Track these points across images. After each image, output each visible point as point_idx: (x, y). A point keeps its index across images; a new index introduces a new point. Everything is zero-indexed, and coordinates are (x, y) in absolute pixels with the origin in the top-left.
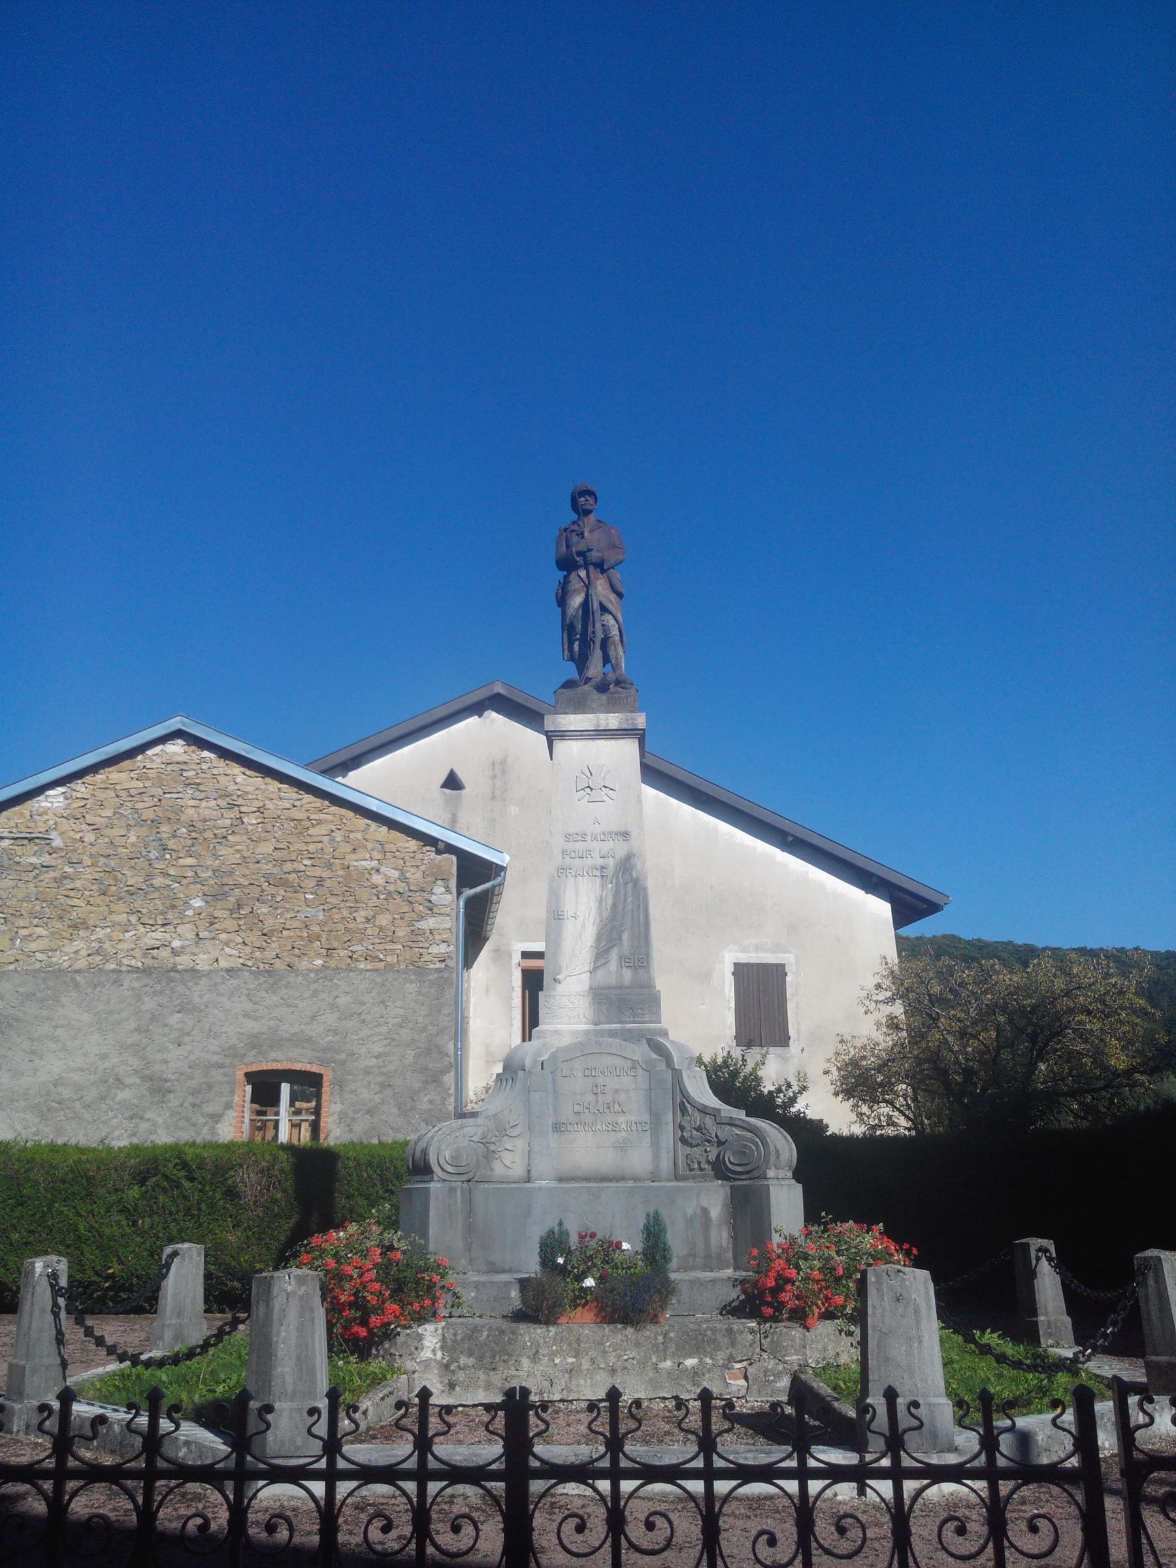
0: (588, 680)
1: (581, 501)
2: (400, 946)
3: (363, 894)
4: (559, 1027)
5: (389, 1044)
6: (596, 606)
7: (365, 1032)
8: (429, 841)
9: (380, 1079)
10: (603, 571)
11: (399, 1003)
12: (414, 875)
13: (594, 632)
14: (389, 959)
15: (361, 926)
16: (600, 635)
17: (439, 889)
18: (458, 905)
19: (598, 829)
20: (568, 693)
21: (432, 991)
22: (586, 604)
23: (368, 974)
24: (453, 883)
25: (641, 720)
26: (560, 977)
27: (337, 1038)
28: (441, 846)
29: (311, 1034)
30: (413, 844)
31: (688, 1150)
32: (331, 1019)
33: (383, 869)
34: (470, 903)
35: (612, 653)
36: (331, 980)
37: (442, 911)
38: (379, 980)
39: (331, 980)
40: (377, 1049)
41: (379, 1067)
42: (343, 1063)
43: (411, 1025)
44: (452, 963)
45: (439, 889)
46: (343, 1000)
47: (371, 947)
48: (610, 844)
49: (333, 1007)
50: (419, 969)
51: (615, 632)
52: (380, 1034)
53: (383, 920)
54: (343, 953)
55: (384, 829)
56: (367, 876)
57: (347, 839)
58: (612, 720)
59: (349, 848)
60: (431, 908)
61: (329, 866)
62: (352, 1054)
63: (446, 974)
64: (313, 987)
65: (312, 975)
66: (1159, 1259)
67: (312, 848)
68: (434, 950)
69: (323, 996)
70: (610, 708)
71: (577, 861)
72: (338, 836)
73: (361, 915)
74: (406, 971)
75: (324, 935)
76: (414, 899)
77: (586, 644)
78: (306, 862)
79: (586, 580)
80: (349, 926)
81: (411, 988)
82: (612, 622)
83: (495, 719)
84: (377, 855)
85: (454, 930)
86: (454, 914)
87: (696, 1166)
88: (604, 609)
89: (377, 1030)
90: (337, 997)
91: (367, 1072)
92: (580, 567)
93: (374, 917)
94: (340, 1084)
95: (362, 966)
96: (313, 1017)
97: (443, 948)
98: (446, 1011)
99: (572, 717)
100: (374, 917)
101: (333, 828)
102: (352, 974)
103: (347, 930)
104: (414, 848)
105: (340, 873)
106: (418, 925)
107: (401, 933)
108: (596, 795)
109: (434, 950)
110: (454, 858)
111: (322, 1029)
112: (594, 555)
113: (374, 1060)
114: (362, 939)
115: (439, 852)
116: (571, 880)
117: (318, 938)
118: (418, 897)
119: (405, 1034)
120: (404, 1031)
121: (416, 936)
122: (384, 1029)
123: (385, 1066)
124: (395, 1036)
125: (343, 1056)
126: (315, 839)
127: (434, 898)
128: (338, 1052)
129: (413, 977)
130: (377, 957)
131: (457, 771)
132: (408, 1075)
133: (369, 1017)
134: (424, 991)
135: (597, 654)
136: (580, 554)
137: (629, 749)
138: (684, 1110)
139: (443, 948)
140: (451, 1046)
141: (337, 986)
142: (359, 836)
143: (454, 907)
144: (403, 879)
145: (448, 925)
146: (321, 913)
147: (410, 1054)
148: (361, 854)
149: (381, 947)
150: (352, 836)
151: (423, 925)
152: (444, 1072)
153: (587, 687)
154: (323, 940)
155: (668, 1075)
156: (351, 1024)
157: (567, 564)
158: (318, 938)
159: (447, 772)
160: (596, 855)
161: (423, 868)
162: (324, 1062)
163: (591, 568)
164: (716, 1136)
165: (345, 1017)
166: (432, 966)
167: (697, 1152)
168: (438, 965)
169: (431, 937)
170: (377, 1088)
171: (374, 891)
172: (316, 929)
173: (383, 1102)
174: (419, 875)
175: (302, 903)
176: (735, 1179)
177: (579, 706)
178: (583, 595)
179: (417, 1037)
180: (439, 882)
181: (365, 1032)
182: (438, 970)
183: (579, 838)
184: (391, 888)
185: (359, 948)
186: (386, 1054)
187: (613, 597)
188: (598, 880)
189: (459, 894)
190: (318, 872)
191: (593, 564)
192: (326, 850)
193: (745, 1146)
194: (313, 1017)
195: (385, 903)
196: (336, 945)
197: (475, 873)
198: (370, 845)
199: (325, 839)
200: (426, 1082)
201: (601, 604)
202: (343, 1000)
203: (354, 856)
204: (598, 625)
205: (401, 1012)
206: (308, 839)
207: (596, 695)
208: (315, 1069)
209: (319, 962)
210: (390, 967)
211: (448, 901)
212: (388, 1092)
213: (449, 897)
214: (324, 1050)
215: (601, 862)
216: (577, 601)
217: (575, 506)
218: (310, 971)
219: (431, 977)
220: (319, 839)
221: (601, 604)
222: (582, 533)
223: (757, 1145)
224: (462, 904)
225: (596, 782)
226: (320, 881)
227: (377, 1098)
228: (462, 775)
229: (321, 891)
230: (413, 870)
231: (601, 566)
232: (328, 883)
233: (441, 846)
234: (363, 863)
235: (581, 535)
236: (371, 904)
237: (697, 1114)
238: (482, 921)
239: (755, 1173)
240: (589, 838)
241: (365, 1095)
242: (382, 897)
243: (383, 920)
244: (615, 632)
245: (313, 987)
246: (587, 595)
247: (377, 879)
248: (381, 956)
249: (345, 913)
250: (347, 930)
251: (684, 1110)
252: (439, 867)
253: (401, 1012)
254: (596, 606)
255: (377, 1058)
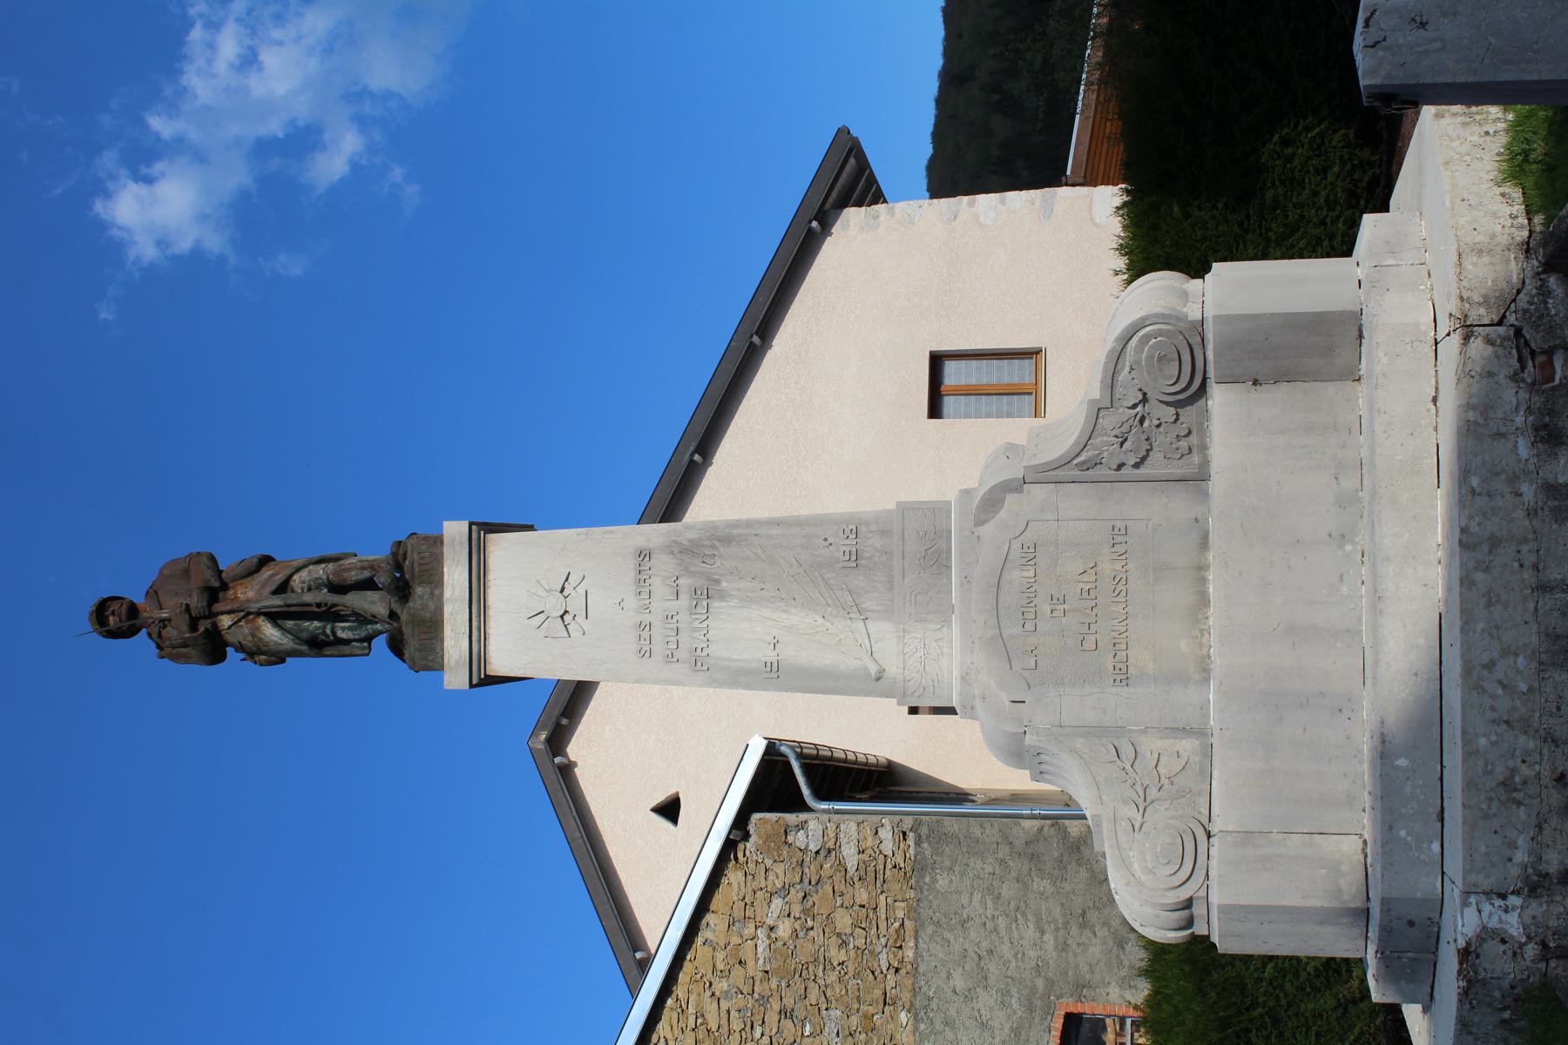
0: (393, 615)
1: (117, 619)
2: (882, 898)
3: (805, 951)
4: (955, 673)
5: (1024, 915)
6: (277, 601)
7: (1006, 950)
8: (729, 847)
9: (1074, 929)
10: (225, 587)
11: (965, 899)
12: (777, 879)
13: (319, 605)
14: (900, 914)
15: (852, 954)
16: (324, 596)
17: (799, 839)
18: (824, 811)
19: (632, 602)
20: (410, 649)
21: (947, 850)
22: (274, 617)
23: (921, 945)
24: (791, 818)
25: (455, 531)
26: (873, 669)
27: (1014, 991)
28: (735, 836)
29: (1006, 1030)
30: (733, 876)
31: (1156, 456)
32: (985, 1000)
33: (770, 922)
34: (821, 796)
35: (354, 576)
36: (930, 999)
37: (832, 835)
38: (930, 929)
39: (930, 999)
40: (1030, 933)
41: (1057, 929)
42: (1050, 984)
43: (996, 883)
44: (908, 822)
45: (799, 839)
46: (959, 982)
47: (883, 941)
48: (656, 582)
49: (969, 996)
50: (917, 870)
51: (320, 571)
52: (1009, 928)
53: (843, 921)
54: (891, 982)
55: (709, 918)
56: (779, 944)
57: (726, 974)
58: (455, 577)
59: (738, 971)
60: (829, 850)
61: (764, 1000)
62: (1038, 968)
63: (924, 831)
64: (939, 1026)
65: (922, 1027)
66: (1219, 907)
67: (736, 1025)
68: (888, 847)
69: (952, 1012)
70: (435, 579)
71: (683, 638)
72: (721, 986)
73: (836, 955)
74: (918, 888)
75: (864, 1008)
76: (814, 875)
77: (331, 614)
78: (757, 1034)
79: (235, 617)
80: (850, 974)
81: (942, 882)
82: (304, 574)
83: (575, 749)
84: (749, 930)
85: (861, 818)
86: (835, 817)
87: (1184, 444)
88: (283, 588)
89: (1003, 932)
90: (954, 991)
91: (1063, 947)
92: (215, 626)
93: (839, 935)
94: (1080, 987)
95: (910, 954)
96: (983, 1026)
97: (886, 834)
98: (977, 831)
99: (449, 643)
100: (839, 935)
101: (708, 993)
102: (920, 970)
103: (857, 975)
104: (740, 874)
105: (774, 983)
106: (852, 869)
107: (862, 896)
108: (575, 604)
109: (888, 847)
110: (756, 817)
111: (1000, 1014)
112: (197, 602)
113: (1046, 938)
114: (871, 952)
115: (746, 836)
116: (714, 650)
117: (869, 1017)
118: (811, 871)
119: (1008, 891)
120: (1005, 892)
121: (870, 873)
122: (1002, 922)
123: (1056, 921)
124: (1013, 904)
125: (1040, 983)
126: (724, 1021)
127: (813, 847)
128: (1034, 989)
129: (927, 880)
130: (897, 931)
131: (654, 803)
132: (1067, 887)
133: (985, 944)
134: (948, 863)
135: (354, 600)
136: (193, 626)
137: (500, 548)
138: (1095, 463)
139: (886, 834)
140: (1026, 824)
141: (939, 990)
142: (720, 956)
143: (826, 817)
144: (785, 890)
145: (853, 826)
146: (832, 1012)
147: (1040, 884)
148: (747, 952)
149: (883, 925)
150: (720, 966)
151: (852, 862)
152: (1065, 833)
153: (404, 617)
154: (871, 1010)
155: (1039, 492)
156: (992, 968)
157: (214, 649)
158: (869, 1017)
159: (654, 816)
160: (673, 606)
161: (768, 862)
162: (1049, 1011)
163: (217, 607)
164: (1134, 406)
165: (983, 980)
166: (912, 851)
167: (1162, 439)
168: (911, 841)
169: (870, 851)
170: (1087, 932)
171: (801, 934)
172: (855, 1021)
173: (1106, 924)
174: (779, 868)
175: (817, 1040)
176: (1204, 380)
177: (433, 626)
178: (261, 621)
179: (1014, 874)
180: (790, 839)
181: (1006, 950)
182: (918, 843)
183: (645, 634)
184: (797, 910)
185: (883, 957)
186: (1038, 915)
187: (266, 573)
188: (715, 604)
189: (809, 809)
190: (772, 1018)
191: (210, 604)
192: (741, 1004)
193: (1150, 357)
194: (983, 1026)
195: (818, 919)
196: (878, 993)
197: (780, 783)
198: (735, 940)
199: (724, 1005)
200: (1079, 862)
201: (275, 592)
202: (959, 982)
203: (751, 963)
204: (308, 598)
205: (977, 897)
206: (724, 1030)
207: (415, 603)
208: (1058, 1024)
209: (903, 1017)
210: (913, 912)
211: (822, 824)
212: (1093, 917)
213: (812, 825)
214: (1031, 1010)
215: (684, 601)
216: (270, 632)
217: (131, 632)
218: (916, 1029)
219: (928, 853)
220: (724, 1014)
221: (275, 592)
222: (162, 621)
223: (1147, 338)
224: (824, 806)
225: (555, 605)
226: (784, 1013)
227: (1102, 932)
228: (659, 798)
229: (800, 1013)
230: (771, 877)
231: (214, 594)
232: (789, 1002)
233: (735, 836)
234: (760, 950)
235: (164, 622)
236: (820, 940)
237: (1096, 441)
238: (871, 773)
239: (1196, 341)
240: (647, 618)
241: (1096, 950)
242: (810, 923)
243: (843, 921)
244: (320, 571)
245: (939, 1026)
246: (259, 614)
247: (784, 930)
248: (897, 925)
249: (832, 977)
250: (857, 975)
251: (1095, 463)
252: (767, 838)
253: (977, 897)
254: (277, 601)
255: (1043, 932)
